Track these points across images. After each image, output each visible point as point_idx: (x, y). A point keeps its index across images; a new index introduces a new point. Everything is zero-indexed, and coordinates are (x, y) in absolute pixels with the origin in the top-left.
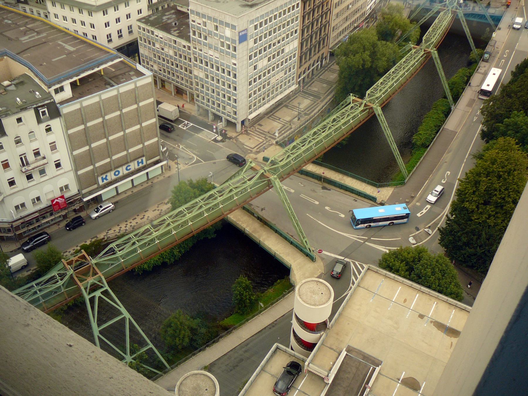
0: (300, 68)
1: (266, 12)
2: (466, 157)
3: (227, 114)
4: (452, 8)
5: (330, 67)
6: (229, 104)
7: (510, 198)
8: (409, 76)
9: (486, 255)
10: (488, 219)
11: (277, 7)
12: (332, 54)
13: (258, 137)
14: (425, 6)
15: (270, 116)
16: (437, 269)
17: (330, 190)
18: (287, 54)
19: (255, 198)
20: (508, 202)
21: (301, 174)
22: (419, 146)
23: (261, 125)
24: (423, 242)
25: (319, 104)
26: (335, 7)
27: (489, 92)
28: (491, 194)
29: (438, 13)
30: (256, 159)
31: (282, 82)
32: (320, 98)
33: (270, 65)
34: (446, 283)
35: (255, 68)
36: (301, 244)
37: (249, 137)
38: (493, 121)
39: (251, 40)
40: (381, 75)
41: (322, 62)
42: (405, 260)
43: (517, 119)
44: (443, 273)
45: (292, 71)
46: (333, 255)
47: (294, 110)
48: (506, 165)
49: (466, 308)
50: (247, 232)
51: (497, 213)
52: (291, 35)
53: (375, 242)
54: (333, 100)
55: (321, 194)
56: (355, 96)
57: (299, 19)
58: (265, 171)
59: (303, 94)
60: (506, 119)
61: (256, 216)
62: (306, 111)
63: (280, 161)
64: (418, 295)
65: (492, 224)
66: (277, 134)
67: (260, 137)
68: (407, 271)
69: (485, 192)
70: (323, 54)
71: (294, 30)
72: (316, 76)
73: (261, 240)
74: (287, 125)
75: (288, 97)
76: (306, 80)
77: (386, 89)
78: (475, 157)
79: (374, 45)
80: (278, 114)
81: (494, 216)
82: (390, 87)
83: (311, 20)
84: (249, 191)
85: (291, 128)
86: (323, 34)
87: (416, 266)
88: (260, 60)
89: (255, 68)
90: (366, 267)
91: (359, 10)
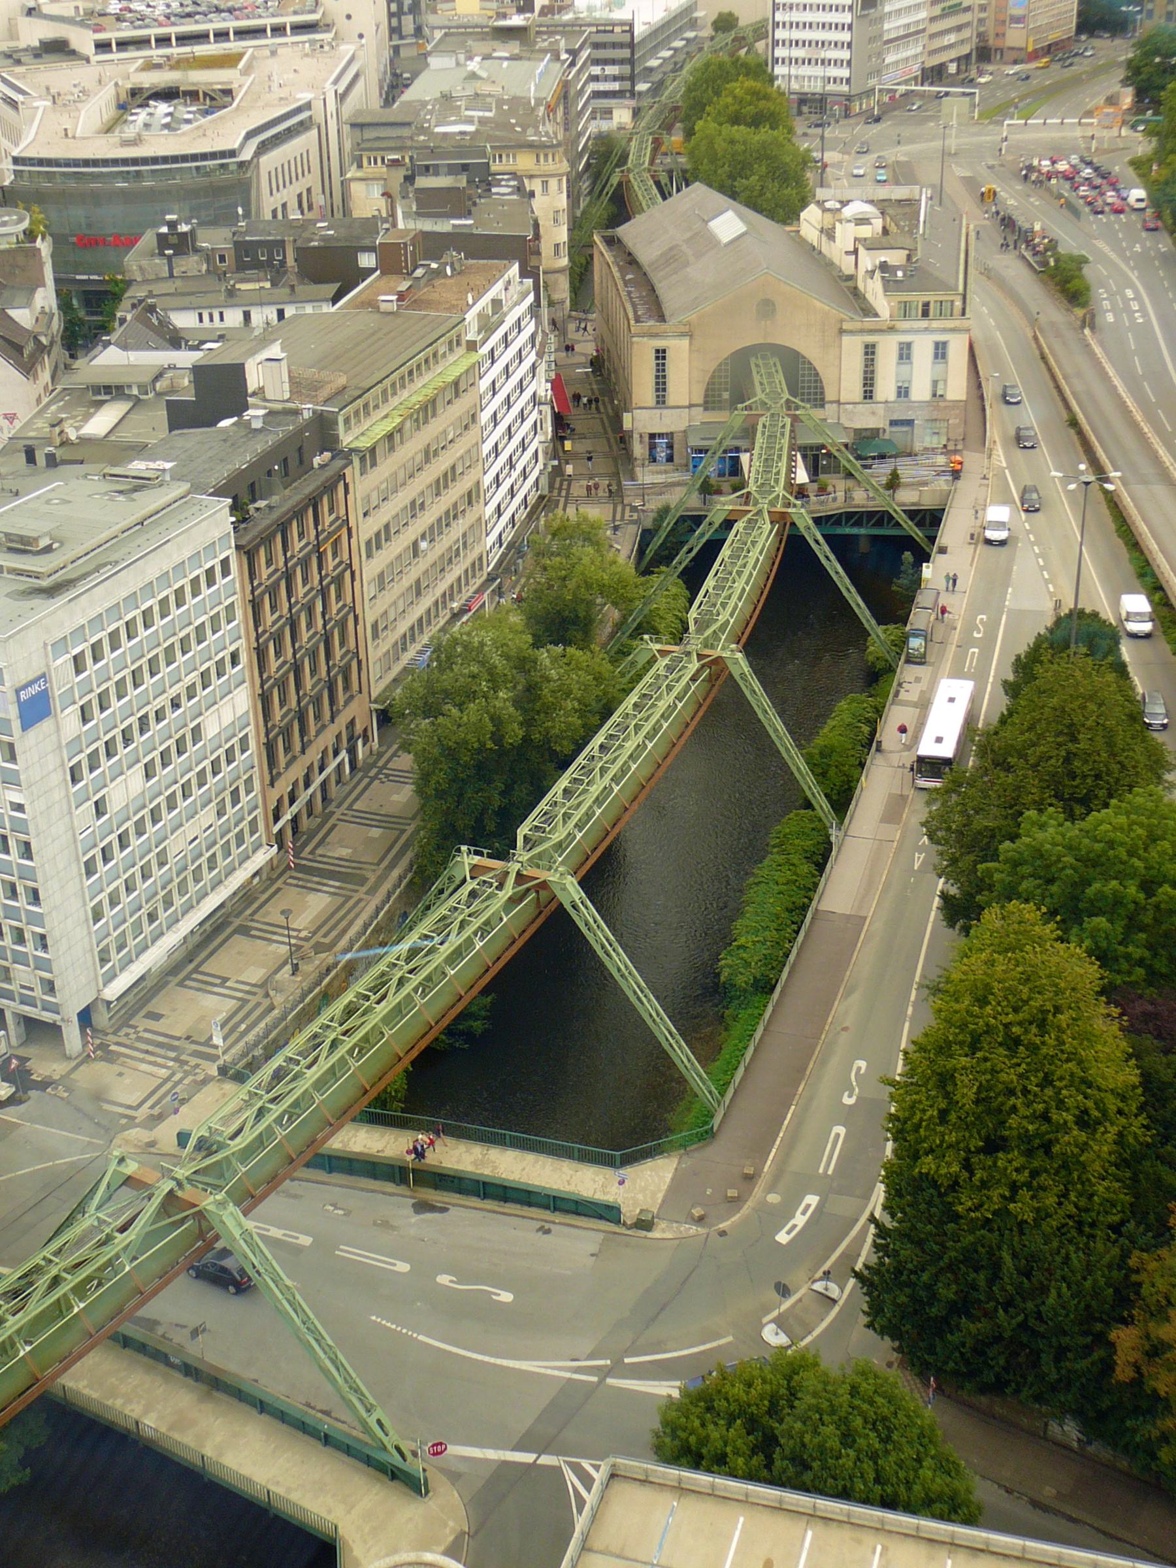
0: (272, 784)
1: (108, 605)
2: (913, 998)
3: (21, 994)
4: (772, 503)
5: (384, 767)
6: (20, 958)
7: (1067, 1110)
8: (662, 750)
9: (1034, 1333)
10: (1012, 1199)
11: (147, 581)
12: (385, 718)
13: (150, 1063)
14: (688, 510)
15: (188, 977)
16: (859, 1422)
17: (444, 1210)
18: (216, 743)
19: (155, 1292)
20: (1064, 1128)
21: (330, 1172)
22: (745, 991)
23: (156, 1017)
24: (816, 1333)
25: (362, 905)
26: (369, 556)
27: (947, 762)
28: (1000, 1111)
29: (728, 524)
30: (152, 1144)
31: (215, 843)
32: (363, 881)
33: (156, 789)
34: (900, 1464)
35: (100, 808)
36: (361, 1436)
37: (116, 1068)
38: (972, 857)
39: (67, 712)
40: (564, 764)
41: (352, 751)
42: (742, 1413)
43: (1040, 835)
44: (883, 1427)
45: (244, 799)
46: (492, 1454)
47: (275, 937)
48: (1025, 997)
49: (987, 1542)
50: (149, 1433)
51: (1034, 1174)
52: (220, 675)
53: (639, 1372)
54: (411, 882)
55: (413, 1232)
56: (477, 853)
57: (239, 613)
58: (180, 1184)
59: (300, 875)
60: (1007, 844)
61: (177, 1361)
62: (318, 938)
63: (232, 1138)
64: (810, 1534)
65: (1029, 1216)
66: (218, 1040)
67: (159, 1060)
68: (754, 1451)
69: (980, 1109)
70: (352, 723)
71: (226, 654)
72: (338, 806)
73: (208, 1452)
74: (254, 1000)
75: (246, 897)
76: (305, 823)
77: (583, 809)
78: (936, 990)
79: (524, 664)
80: (216, 965)
81: (1029, 1186)
82: (598, 801)
83: (285, 610)
84: (127, 1268)
85: (272, 1008)
86: (338, 653)
87: (784, 1426)
88: (112, 780)
89: (100, 808)
90: (605, 1468)
91: (457, 554)
